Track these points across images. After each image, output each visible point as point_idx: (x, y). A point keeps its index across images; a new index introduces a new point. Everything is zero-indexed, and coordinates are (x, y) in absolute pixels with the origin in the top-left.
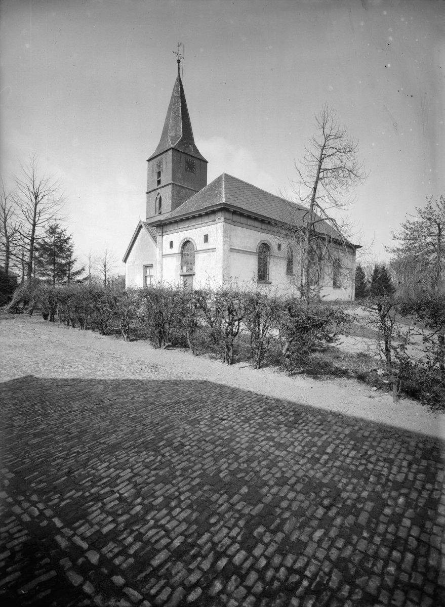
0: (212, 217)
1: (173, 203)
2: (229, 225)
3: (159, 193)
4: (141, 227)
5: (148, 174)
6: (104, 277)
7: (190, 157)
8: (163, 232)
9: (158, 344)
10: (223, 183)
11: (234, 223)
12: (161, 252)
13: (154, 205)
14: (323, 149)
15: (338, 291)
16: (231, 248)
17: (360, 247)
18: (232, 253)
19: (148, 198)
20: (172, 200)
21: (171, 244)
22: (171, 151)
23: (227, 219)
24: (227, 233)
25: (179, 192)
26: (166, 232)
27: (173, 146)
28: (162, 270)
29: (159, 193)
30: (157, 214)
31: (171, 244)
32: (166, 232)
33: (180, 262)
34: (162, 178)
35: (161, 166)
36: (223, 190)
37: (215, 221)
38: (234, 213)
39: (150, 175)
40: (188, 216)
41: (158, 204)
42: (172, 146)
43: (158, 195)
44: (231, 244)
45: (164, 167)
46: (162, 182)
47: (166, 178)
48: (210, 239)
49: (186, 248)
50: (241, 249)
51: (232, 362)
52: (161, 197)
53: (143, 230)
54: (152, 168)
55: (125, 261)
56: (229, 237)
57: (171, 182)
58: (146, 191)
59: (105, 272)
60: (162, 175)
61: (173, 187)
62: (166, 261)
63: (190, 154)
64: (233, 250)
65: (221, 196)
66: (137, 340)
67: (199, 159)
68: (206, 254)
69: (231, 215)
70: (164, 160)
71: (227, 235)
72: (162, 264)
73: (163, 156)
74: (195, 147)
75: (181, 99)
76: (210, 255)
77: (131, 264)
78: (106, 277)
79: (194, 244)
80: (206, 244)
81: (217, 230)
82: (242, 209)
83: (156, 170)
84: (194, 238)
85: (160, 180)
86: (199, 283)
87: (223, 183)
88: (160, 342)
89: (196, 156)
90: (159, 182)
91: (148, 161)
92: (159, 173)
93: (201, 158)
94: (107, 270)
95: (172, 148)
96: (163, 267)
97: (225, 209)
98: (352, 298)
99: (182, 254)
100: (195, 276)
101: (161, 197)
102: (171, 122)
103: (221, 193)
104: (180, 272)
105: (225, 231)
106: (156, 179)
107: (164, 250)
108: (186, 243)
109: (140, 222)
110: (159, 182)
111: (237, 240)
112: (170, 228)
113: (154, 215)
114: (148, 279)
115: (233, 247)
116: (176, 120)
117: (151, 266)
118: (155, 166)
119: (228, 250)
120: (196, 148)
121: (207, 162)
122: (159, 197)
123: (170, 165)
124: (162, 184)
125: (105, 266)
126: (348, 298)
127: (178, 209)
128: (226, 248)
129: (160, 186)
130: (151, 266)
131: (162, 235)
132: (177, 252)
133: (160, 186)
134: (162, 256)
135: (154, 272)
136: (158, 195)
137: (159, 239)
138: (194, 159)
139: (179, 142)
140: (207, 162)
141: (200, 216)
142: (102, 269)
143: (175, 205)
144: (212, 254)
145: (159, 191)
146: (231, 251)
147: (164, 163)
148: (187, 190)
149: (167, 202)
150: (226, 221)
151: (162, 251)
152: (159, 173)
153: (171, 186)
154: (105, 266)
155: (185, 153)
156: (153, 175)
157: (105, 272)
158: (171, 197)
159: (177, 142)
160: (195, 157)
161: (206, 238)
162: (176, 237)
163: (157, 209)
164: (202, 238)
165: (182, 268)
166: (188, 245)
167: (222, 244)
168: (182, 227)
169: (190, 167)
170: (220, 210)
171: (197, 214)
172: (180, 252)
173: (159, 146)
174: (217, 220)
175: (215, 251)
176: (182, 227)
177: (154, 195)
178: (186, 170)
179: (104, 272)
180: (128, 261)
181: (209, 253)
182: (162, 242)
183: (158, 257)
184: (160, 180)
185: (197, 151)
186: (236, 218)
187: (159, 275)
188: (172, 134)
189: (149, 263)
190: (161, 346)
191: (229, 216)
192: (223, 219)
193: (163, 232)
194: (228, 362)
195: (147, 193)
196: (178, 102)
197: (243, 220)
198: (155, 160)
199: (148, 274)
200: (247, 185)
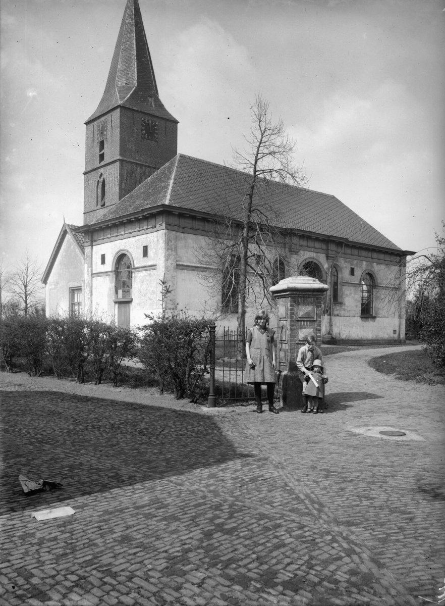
0: (152, 222)
1: (121, 189)
2: (174, 233)
3: (101, 175)
4: (64, 234)
6: (25, 304)
7: (149, 118)
8: (92, 241)
9: (34, 372)
10: (174, 171)
11: (182, 229)
14: (259, 146)
15: (370, 324)
16: (177, 265)
17: (412, 253)
18: (179, 272)
19: (86, 181)
20: (120, 185)
21: (103, 257)
22: (118, 110)
23: (170, 225)
24: (170, 243)
25: (131, 173)
28: (91, 295)
29: (101, 175)
30: (99, 207)
31: (103, 257)
32: (97, 241)
33: (113, 284)
34: (106, 150)
36: (171, 182)
37: (155, 227)
39: (89, 147)
40: (122, 220)
41: (100, 190)
42: (120, 102)
43: (100, 177)
44: (178, 259)
47: (113, 151)
48: (150, 252)
50: (193, 265)
52: (104, 179)
53: (69, 237)
54: (92, 136)
55: (45, 281)
57: (119, 157)
58: (84, 170)
59: (26, 297)
60: (105, 146)
61: (121, 165)
62: (98, 281)
63: (150, 112)
64: (179, 267)
65: (166, 192)
66: (20, 372)
67: (163, 119)
68: (145, 273)
69: (176, 219)
70: (109, 123)
71: (171, 247)
72: (92, 287)
73: (108, 117)
75: (136, 27)
78: (27, 305)
79: (130, 257)
80: (145, 258)
81: (158, 240)
83: (97, 139)
84: (131, 250)
85: (103, 154)
86: (85, 313)
87: (174, 171)
88: (36, 371)
89: (157, 114)
90: (102, 157)
91: (87, 123)
92: (102, 144)
93: (166, 117)
95: (119, 106)
97: (166, 212)
99: (117, 272)
100: (132, 303)
101: (104, 181)
103: (167, 187)
105: (168, 242)
108: (121, 258)
109: (65, 225)
110: (102, 157)
111: (187, 253)
114: (76, 307)
115: (181, 263)
116: (127, 61)
117: (79, 289)
118: (96, 133)
119: (172, 268)
120: (159, 101)
122: (102, 179)
123: (117, 131)
124: (107, 159)
125: (26, 286)
126: (392, 335)
128: (170, 265)
129: (103, 163)
130: (79, 289)
132: (110, 270)
133: (103, 163)
134: (92, 274)
136: (100, 177)
137: (88, 250)
138: (155, 119)
140: (176, 122)
141: (138, 220)
142: (21, 291)
143: (126, 188)
144: (153, 272)
145: (101, 171)
146: (177, 269)
147: (109, 127)
148: (145, 168)
149: (113, 189)
150: (170, 227)
151: (92, 267)
152: (102, 144)
153: (118, 164)
154: (26, 286)
155: (141, 112)
157: (26, 297)
159: (128, 96)
162: (109, 248)
163: (100, 199)
164: (141, 251)
165: (117, 292)
166: (125, 259)
167: (163, 259)
168: (116, 234)
169: (150, 131)
170: (160, 213)
171: (132, 218)
172: (114, 269)
173: (103, 100)
174: (158, 226)
175: (156, 269)
176: (116, 234)
177: (94, 176)
179: (24, 297)
181: (148, 272)
183: (87, 277)
185: (161, 106)
188: (121, 82)
189: (75, 284)
190: (36, 374)
191: (174, 220)
192: (164, 225)
193: (92, 241)
195: (85, 173)
196: (131, 32)
198: (95, 123)
200: (216, 169)
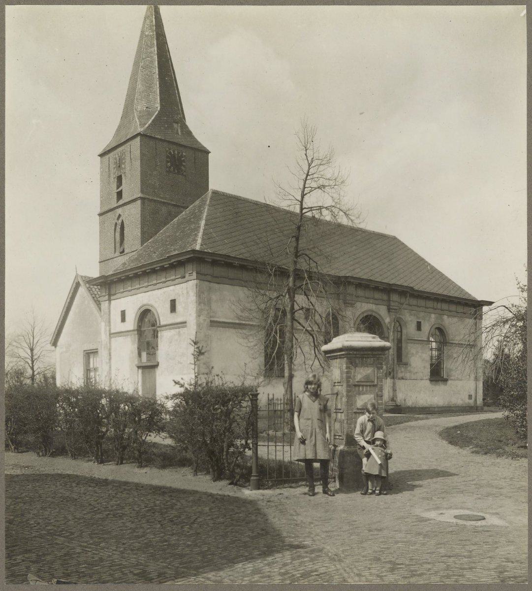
0: (180, 271)
2: (207, 283)
3: (120, 216)
4: (77, 286)
5: (102, 181)
8: (110, 295)
10: (206, 210)
12: (108, 328)
13: (113, 236)
15: (440, 388)
16: (211, 321)
20: (142, 228)
21: (123, 314)
22: (138, 139)
26: (115, 294)
27: (142, 129)
28: (110, 359)
29: (120, 216)
30: (118, 254)
31: (123, 314)
33: (136, 346)
34: (124, 187)
35: (123, 166)
36: (203, 223)
38: (214, 263)
39: (104, 183)
42: (140, 130)
43: (118, 219)
44: (212, 314)
45: (127, 166)
46: (124, 195)
47: (132, 188)
48: (179, 307)
49: (146, 320)
51: (102, 462)
53: (82, 290)
54: (107, 170)
55: (55, 343)
56: (209, 302)
57: (140, 195)
58: (98, 211)
59: (33, 362)
60: (124, 181)
61: (143, 204)
62: (117, 342)
64: (214, 324)
66: (27, 451)
67: (192, 148)
68: (173, 332)
71: (203, 301)
72: (110, 349)
73: (125, 148)
74: (184, 127)
76: (179, 333)
77: (64, 350)
79: (155, 314)
82: (229, 256)
84: (156, 305)
85: (121, 190)
87: (206, 210)
90: (120, 195)
91: (101, 155)
92: (119, 179)
93: (194, 146)
94: (35, 357)
95: (139, 134)
96: (112, 354)
98: (476, 400)
99: (140, 331)
101: (123, 222)
102: (140, 86)
104: (136, 362)
105: (200, 294)
106: (115, 190)
107: (112, 327)
108: (145, 314)
110: (120, 195)
112: (120, 288)
113: (112, 256)
115: (215, 319)
117: (95, 352)
118: (112, 166)
121: (208, 152)
122: (120, 221)
124: (126, 198)
125: (32, 350)
126: (467, 401)
127: (165, 231)
128: (202, 322)
129: (121, 202)
130: (95, 352)
131: (110, 300)
133: (121, 202)
134: (110, 334)
135: (98, 362)
136: (118, 219)
137: (104, 305)
139: (153, 121)
140: (208, 152)
144: (182, 330)
145: (119, 211)
146: (211, 326)
149: (133, 232)
152: (119, 179)
153: (139, 202)
154: (32, 350)
155: (164, 141)
156: (109, 183)
157: (33, 362)
158: (139, 222)
159: (150, 122)
160: (185, 147)
161: (173, 303)
163: (118, 245)
164: (168, 306)
165: (140, 355)
166: (149, 316)
167: (194, 315)
170: (189, 261)
172: (136, 328)
174: (187, 275)
177: (111, 217)
178: (169, 172)
179: (30, 362)
180: (59, 344)
181: (177, 330)
182: (110, 311)
183: (104, 337)
184: (121, 190)
185: (189, 133)
186: (218, 271)
187: (105, 367)
188: (140, 106)
191: (206, 269)
192: (195, 274)
193: (110, 295)
194: (98, 462)
195: (100, 215)
197: (232, 273)
198: (111, 155)
199: (91, 366)
